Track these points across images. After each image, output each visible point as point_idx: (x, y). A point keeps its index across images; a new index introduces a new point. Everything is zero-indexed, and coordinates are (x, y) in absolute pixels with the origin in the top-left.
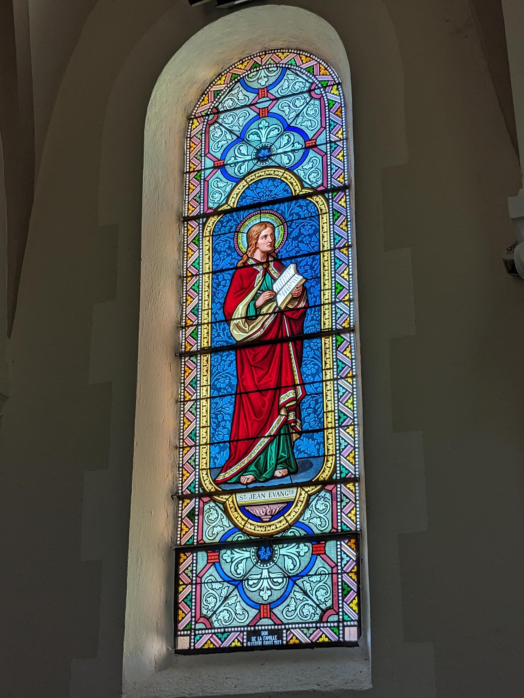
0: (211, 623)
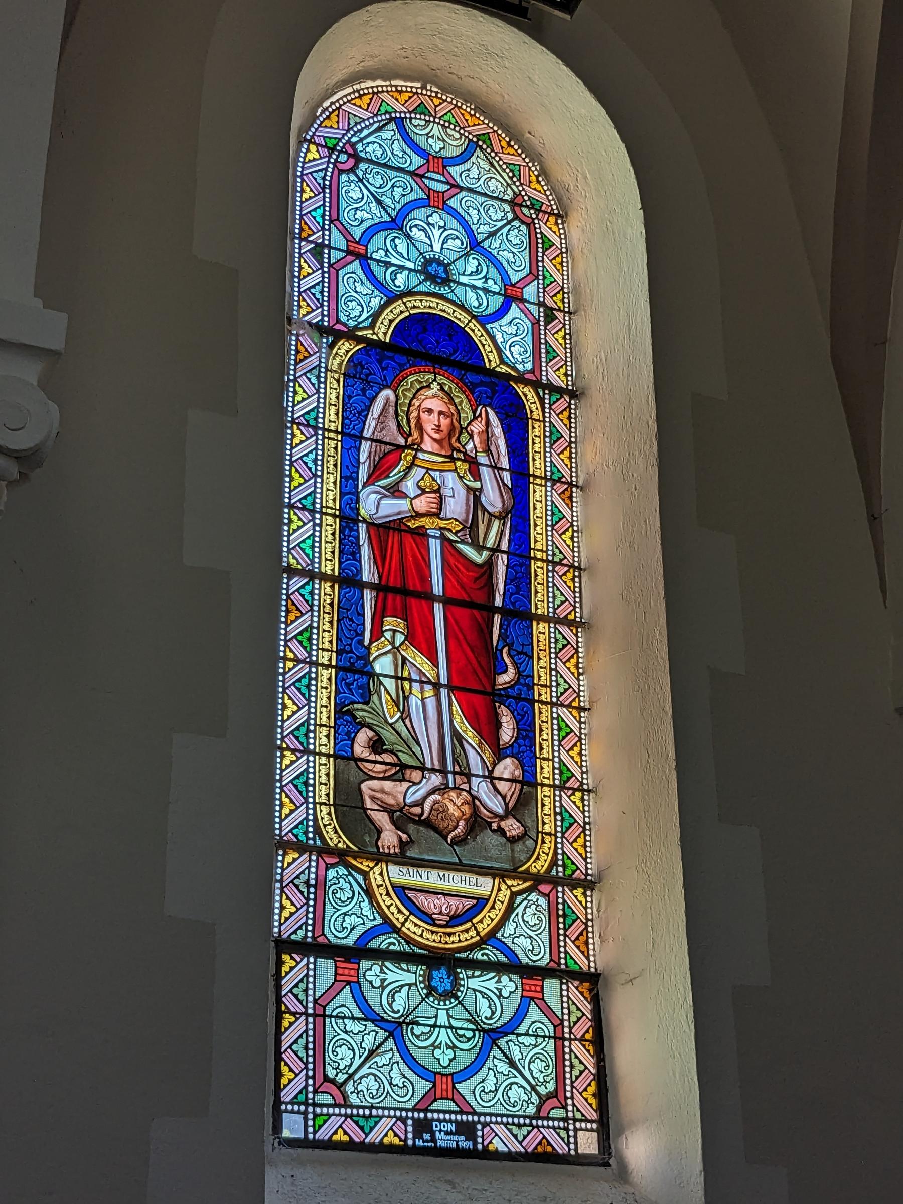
0: (345, 1097)
